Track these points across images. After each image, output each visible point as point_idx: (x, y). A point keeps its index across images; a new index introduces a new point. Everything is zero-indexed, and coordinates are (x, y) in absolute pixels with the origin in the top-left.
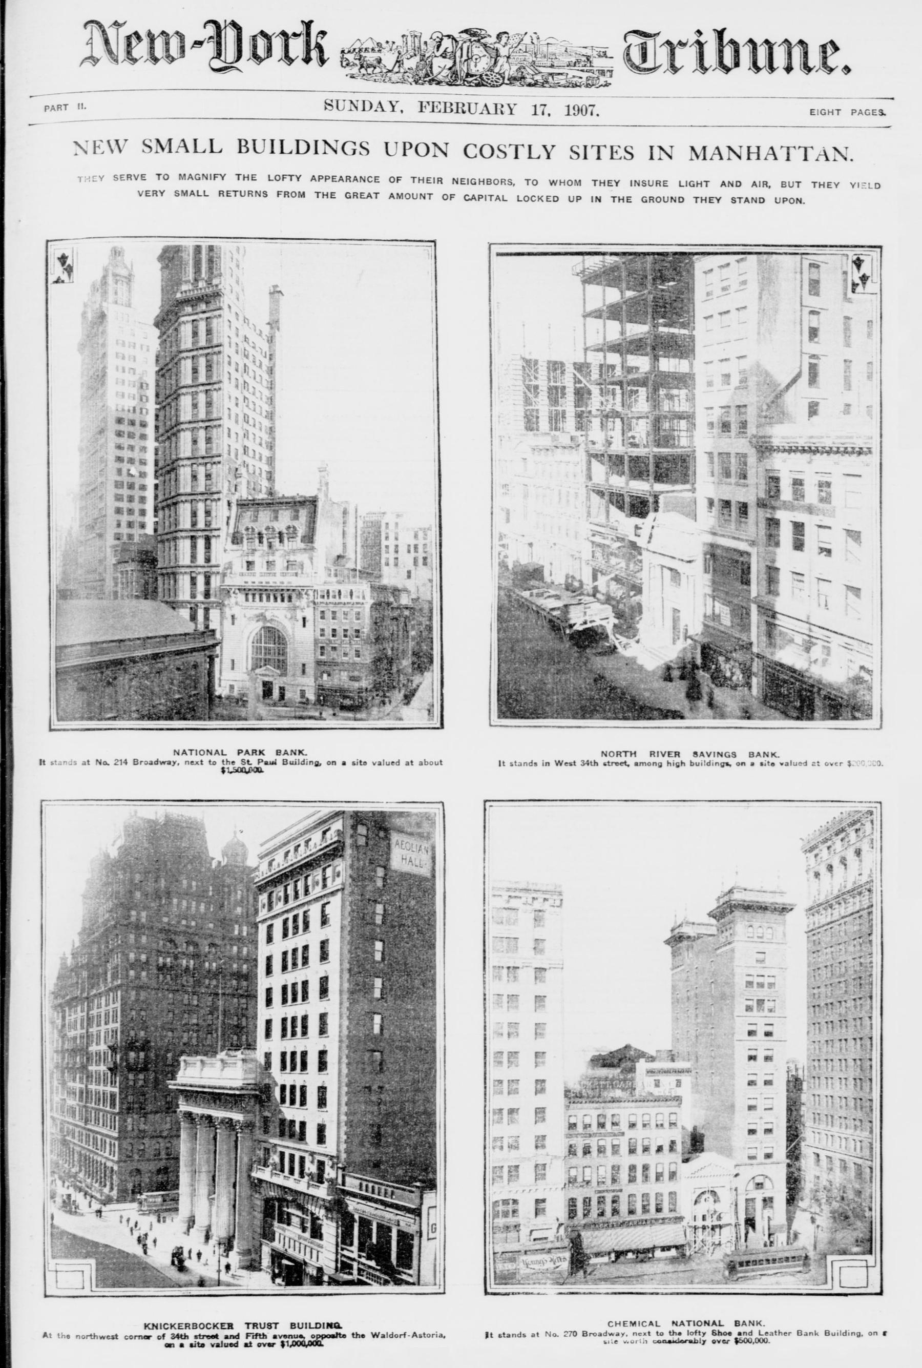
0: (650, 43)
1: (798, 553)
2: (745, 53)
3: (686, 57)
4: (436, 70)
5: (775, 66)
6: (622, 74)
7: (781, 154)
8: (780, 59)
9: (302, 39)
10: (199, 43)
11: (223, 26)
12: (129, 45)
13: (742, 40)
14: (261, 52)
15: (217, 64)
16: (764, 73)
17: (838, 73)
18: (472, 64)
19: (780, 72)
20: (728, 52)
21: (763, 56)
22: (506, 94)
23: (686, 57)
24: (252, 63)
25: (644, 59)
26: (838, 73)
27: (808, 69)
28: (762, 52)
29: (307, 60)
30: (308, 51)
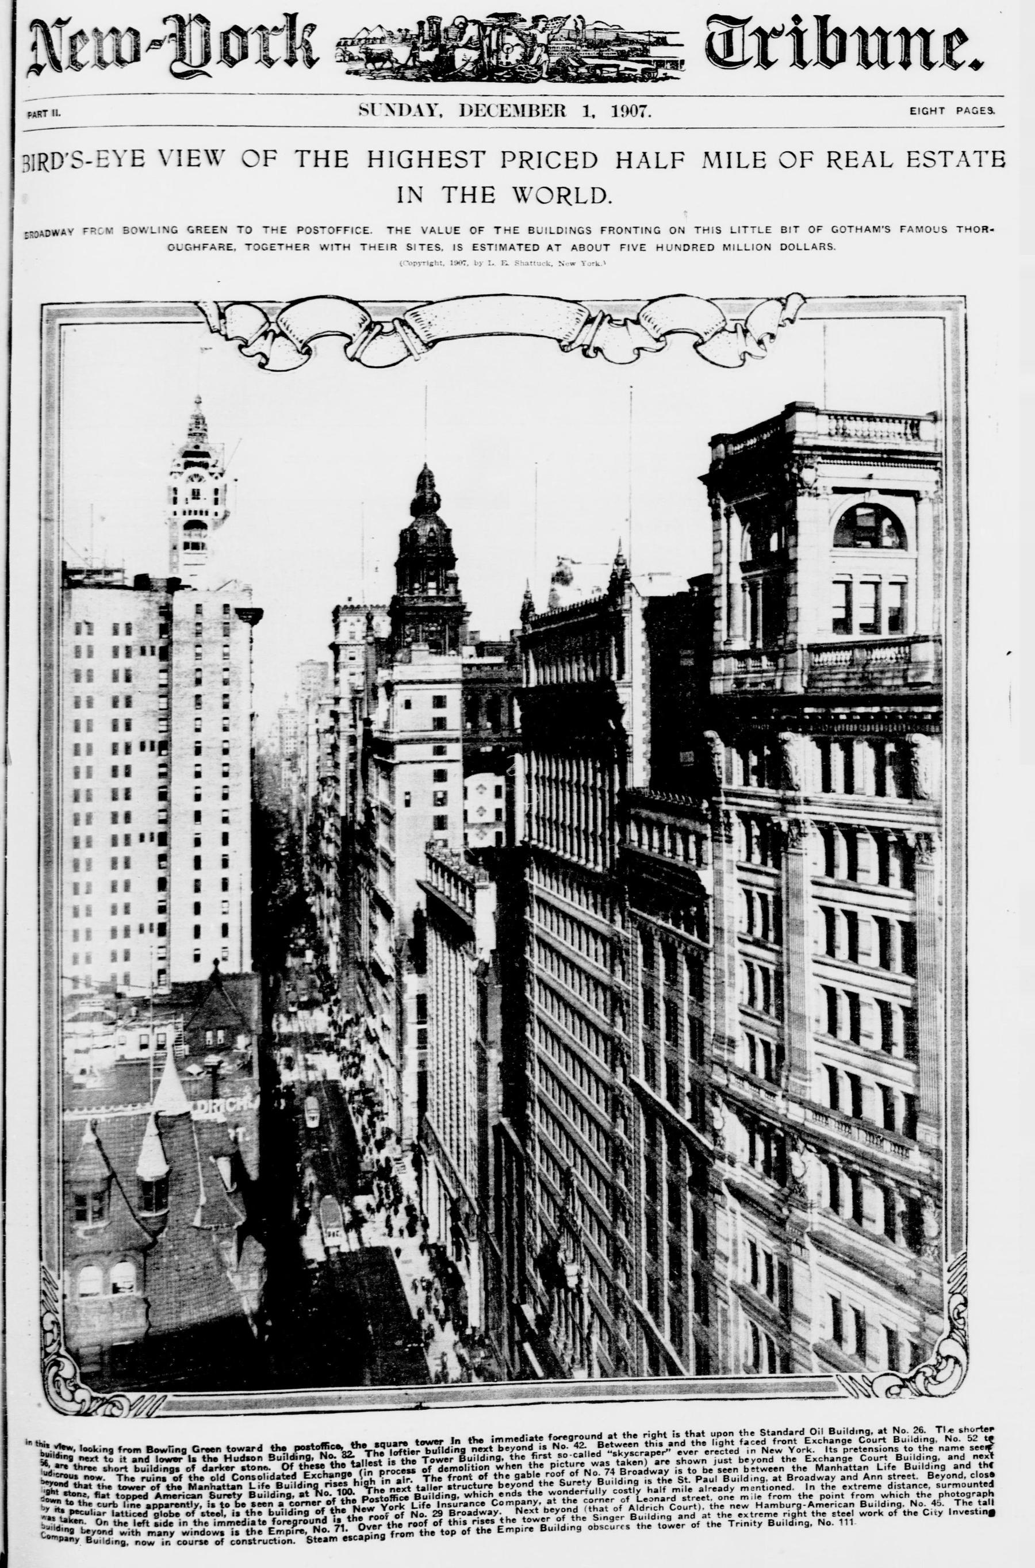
0: (737, 33)
1: (432, 777)
2: (853, 44)
3: (781, 48)
4: (458, 64)
5: (890, 61)
6: (698, 70)
7: (973, 159)
8: (895, 51)
9: (285, 34)
10: (157, 43)
11: (187, 21)
12: (73, 47)
13: (849, 29)
14: (234, 52)
15: (180, 67)
16: (876, 68)
17: (965, 69)
18: (502, 55)
19: (896, 68)
20: (832, 42)
21: (876, 48)
22: (544, 91)
23: (781, 48)
24: (223, 66)
25: (730, 51)
26: (965, 69)
27: (928, 64)
28: (874, 44)
29: (291, 61)
30: (292, 50)
